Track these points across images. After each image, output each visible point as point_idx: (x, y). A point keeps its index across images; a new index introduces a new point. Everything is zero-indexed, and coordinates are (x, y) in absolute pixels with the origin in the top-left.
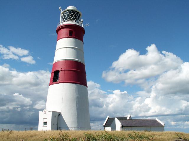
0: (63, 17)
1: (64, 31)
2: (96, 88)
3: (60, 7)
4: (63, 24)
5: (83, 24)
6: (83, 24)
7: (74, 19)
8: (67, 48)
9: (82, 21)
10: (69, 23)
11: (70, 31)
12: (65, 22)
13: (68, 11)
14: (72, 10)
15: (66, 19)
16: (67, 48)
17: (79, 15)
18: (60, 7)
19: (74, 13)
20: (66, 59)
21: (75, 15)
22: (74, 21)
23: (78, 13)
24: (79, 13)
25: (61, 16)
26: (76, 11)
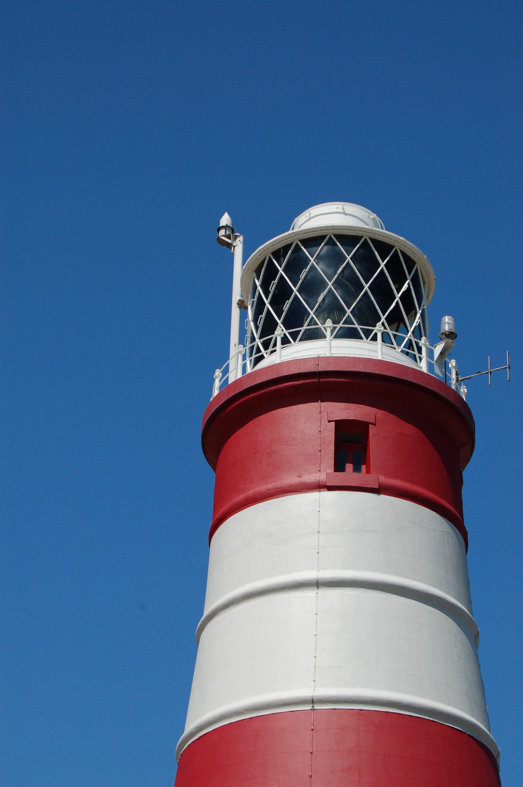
0: (260, 305)
1: (309, 428)
2: (313, 706)
3: (225, 220)
4: (261, 365)
5: (452, 363)
6: (452, 363)
7: (367, 316)
8: (318, 584)
9: (451, 335)
10: (326, 353)
11: (341, 426)
12: (285, 341)
13: (312, 240)
14: (348, 239)
15: (295, 318)
16: (318, 584)
17: (415, 281)
18: (225, 220)
19: (366, 261)
20: (313, 701)
21: (378, 282)
22: (378, 329)
23: (401, 266)
24: (411, 263)
25: (236, 296)
26: (384, 248)
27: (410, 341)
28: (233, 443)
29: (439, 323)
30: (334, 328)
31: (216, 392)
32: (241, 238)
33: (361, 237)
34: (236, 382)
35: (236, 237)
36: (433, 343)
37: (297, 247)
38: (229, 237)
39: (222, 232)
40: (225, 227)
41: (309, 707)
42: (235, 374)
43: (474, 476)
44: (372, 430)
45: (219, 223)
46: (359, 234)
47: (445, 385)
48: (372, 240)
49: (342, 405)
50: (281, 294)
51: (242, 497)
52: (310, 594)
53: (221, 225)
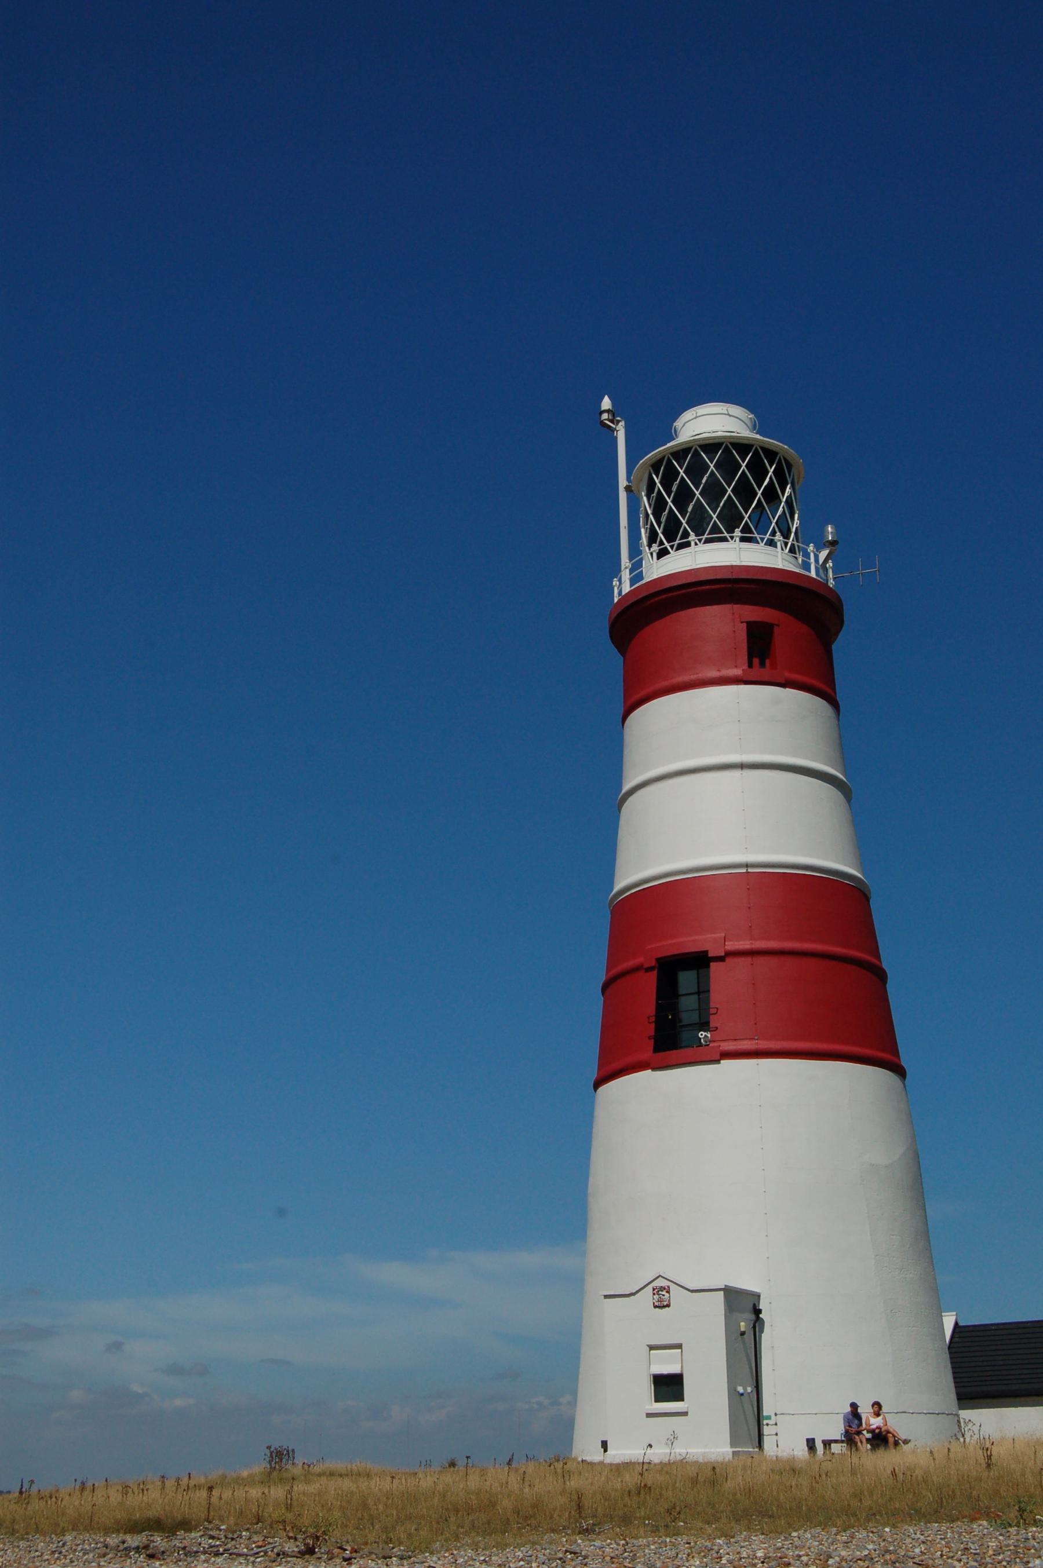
1: (719, 624)
3: (606, 403)
8: (742, 766)
9: (833, 543)
16: (742, 766)
20: (747, 866)
27: (793, 545)
28: (648, 643)
29: (823, 532)
30: (786, 544)
31: (616, 600)
32: (622, 423)
33: (752, 446)
34: (624, 598)
35: (618, 422)
36: (819, 548)
37: (696, 454)
38: (612, 421)
39: (605, 416)
40: (608, 411)
41: (744, 870)
42: (626, 588)
43: (844, 649)
44: (776, 630)
45: (600, 406)
46: (751, 442)
47: (825, 585)
48: (761, 448)
49: (747, 608)
50: (683, 497)
51: (665, 684)
52: (736, 774)
53: (603, 409)
